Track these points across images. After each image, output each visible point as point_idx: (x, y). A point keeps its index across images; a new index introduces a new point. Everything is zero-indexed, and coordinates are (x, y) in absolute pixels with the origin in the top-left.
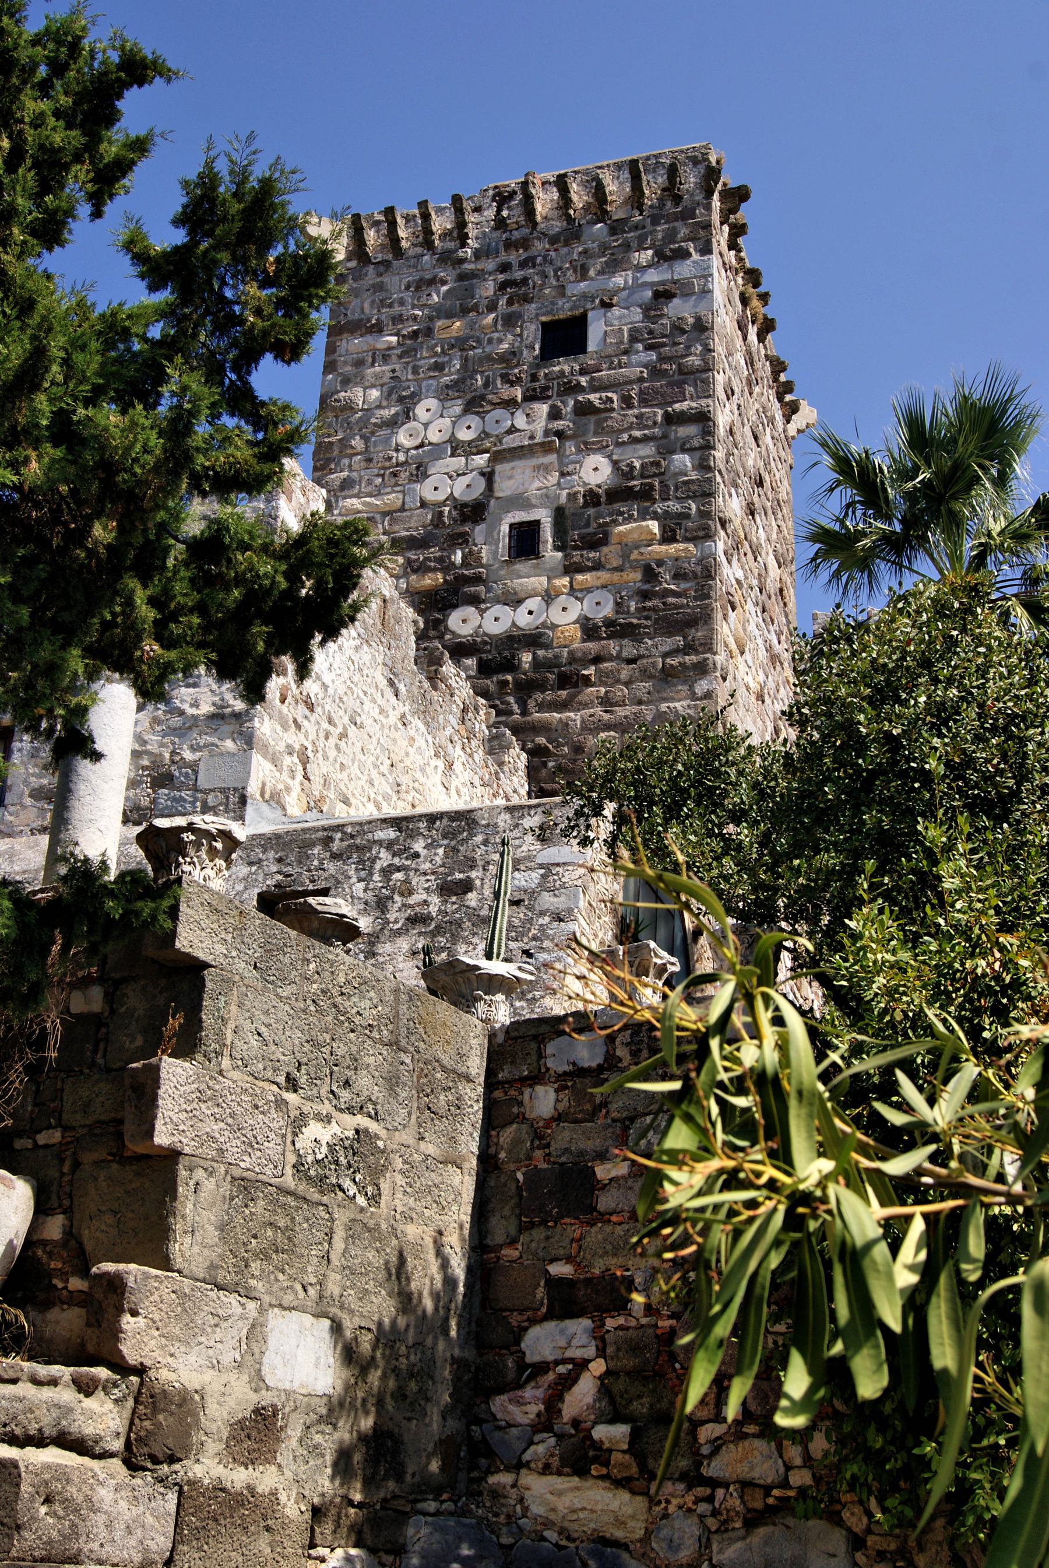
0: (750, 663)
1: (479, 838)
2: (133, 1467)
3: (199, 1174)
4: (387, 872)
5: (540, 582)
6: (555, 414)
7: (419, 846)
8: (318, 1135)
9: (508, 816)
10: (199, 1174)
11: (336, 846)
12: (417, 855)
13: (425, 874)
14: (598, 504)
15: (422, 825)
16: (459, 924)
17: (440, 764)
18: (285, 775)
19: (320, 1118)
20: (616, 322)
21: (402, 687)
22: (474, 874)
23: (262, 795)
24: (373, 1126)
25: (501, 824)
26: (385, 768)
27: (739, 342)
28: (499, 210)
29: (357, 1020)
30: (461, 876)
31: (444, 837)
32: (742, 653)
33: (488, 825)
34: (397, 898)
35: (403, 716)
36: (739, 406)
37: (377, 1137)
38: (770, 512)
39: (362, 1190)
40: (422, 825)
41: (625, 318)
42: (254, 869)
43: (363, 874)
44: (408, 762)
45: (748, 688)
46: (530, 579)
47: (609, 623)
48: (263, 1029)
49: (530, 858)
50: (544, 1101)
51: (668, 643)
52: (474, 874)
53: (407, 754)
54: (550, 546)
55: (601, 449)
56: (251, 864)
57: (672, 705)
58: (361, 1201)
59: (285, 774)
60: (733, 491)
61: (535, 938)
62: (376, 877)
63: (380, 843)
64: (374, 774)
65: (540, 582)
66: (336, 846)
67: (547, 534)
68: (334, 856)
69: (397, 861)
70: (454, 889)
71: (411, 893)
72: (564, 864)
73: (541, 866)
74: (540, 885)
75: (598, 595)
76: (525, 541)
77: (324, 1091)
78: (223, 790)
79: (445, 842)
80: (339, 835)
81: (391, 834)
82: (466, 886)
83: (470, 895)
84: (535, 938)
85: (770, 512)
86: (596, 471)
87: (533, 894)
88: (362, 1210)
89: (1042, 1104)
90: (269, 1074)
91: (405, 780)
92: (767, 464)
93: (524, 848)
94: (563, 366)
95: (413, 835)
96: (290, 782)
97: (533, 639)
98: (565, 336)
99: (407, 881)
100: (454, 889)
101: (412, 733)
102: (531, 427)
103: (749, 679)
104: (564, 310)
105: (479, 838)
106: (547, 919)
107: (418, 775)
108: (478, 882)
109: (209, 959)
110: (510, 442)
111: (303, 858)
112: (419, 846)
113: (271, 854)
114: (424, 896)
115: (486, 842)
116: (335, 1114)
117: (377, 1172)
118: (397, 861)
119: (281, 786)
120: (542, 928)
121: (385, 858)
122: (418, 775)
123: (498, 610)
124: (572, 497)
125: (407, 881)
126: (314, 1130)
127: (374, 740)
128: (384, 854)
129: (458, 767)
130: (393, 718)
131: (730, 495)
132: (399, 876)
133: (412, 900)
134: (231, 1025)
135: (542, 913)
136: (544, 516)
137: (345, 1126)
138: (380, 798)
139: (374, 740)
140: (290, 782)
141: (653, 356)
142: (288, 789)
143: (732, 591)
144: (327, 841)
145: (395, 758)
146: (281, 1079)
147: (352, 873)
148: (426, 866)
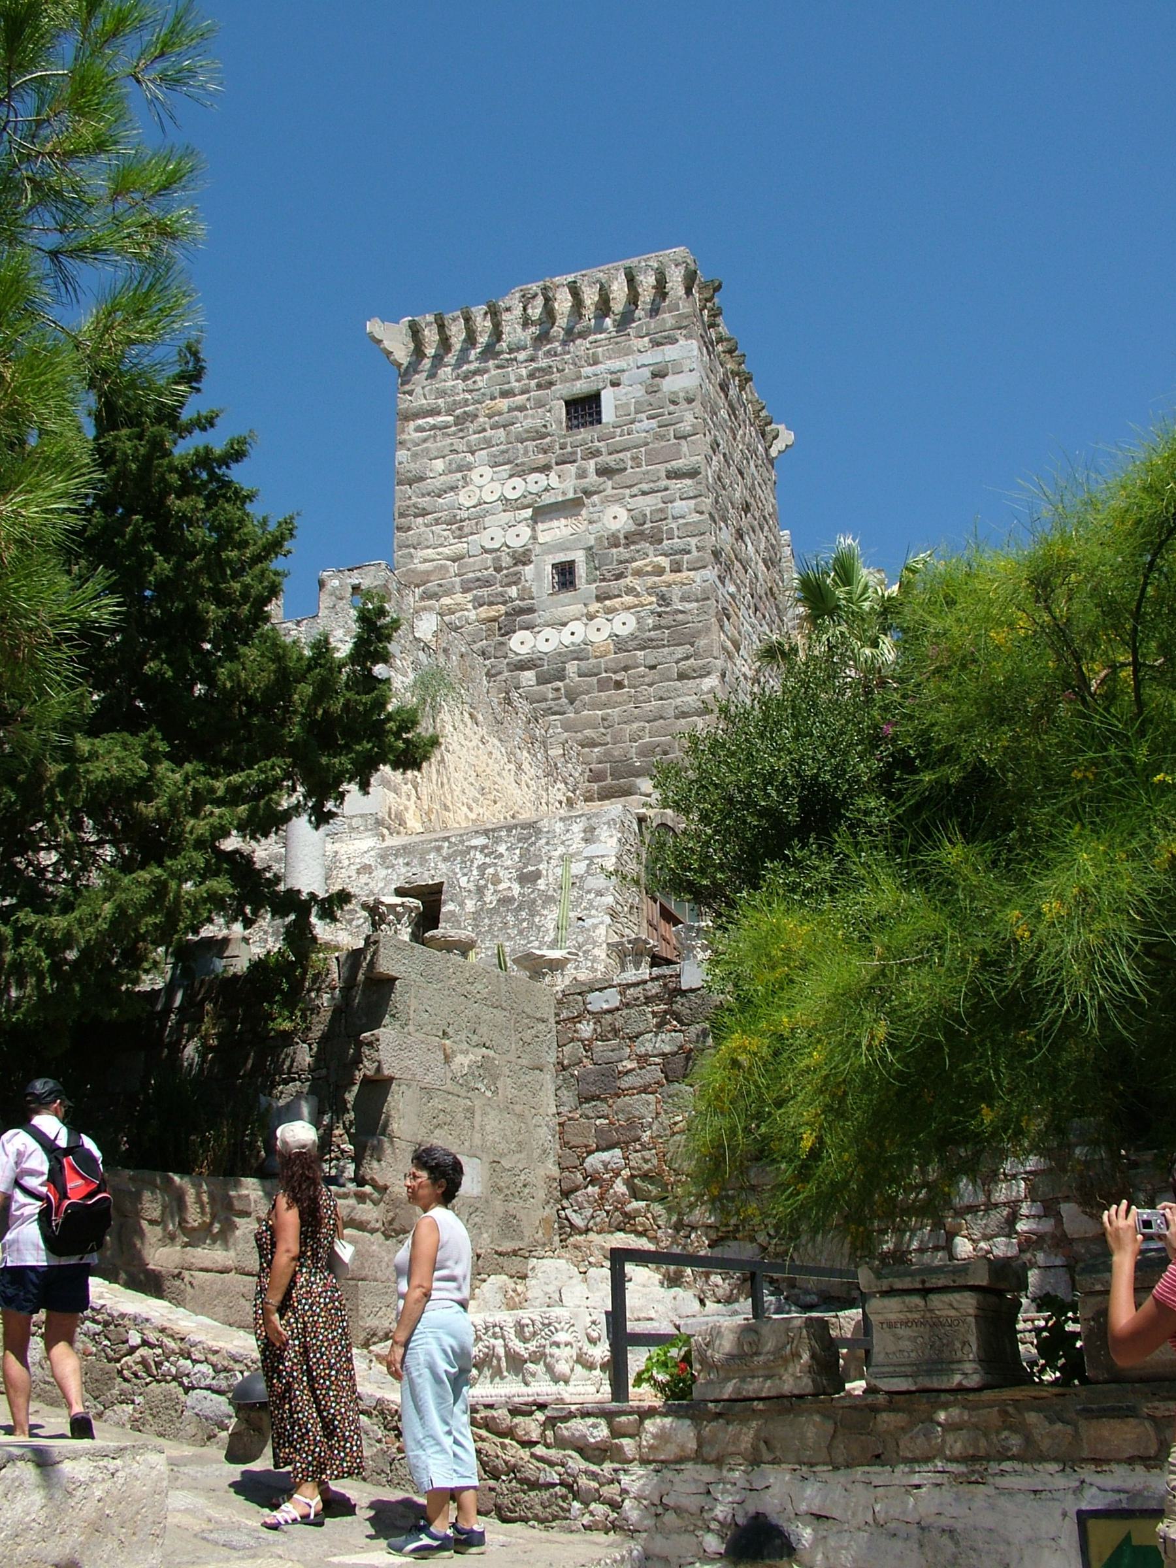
0: (746, 657)
1: (543, 841)
2: (387, 1237)
3: (404, 1087)
4: (482, 868)
5: (578, 608)
6: (582, 474)
7: (502, 849)
8: (463, 1061)
9: (562, 824)
10: (404, 1087)
11: (445, 852)
12: (501, 855)
13: (507, 869)
14: (617, 546)
15: (503, 833)
16: (534, 901)
17: (512, 766)
18: (404, 800)
19: (462, 1052)
20: (623, 398)
21: (480, 717)
22: (541, 867)
23: (390, 817)
24: (491, 1053)
25: (558, 830)
26: (472, 780)
27: (722, 402)
28: (525, 309)
29: (478, 996)
30: (533, 868)
31: (519, 840)
32: (738, 650)
33: (548, 832)
34: (489, 885)
35: (483, 737)
36: (724, 455)
37: (494, 1059)
38: (757, 528)
39: (488, 1088)
40: (503, 833)
41: (630, 392)
42: (390, 871)
43: (465, 870)
44: (488, 771)
45: (746, 678)
46: (568, 605)
47: (633, 637)
48: (428, 1008)
49: (579, 853)
50: (586, 1029)
51: (680, 652)
52: (541, 867)
53: (487, 765)
54: (583, 580)
55: (619, 500)
56: (387, 868)
57: (684, 699)
58: (489, 1094)
59: (404, 797)
60: (722, 524)
61: (586, 909)
62: (475, 872)
63: (475, 847)
64: (466, 785)
65: (578, 608)
66: (445, 852)
67: (581, 570)
68: (445, 860)
69: (488, 860)
70: (528, 879)
71: (499, 882)
72: (603, 856)
73: (587, 858)
74: (587, 872)
75: (625, 616)
76: (565, 575)
77: (464, 1038)
78: (362, 816)
79: (520, 845)
80: (446, 844)
81: (481, 841)
82: (537, 875)
83: (539, 882)
84: (586, 909)
85: (757, 528)
86: (617, 519)
87: (581, 878)
88: (489, 1099)
89: (1175, 936)
90: (434, 1032)
91: (487, 784)
92: (751, 489)
93: (574, 846)
94: (584, 434)
95: (497, 841)
96: (407, 803)
97: (578, 654)
98: (584, 409)
99: (496, 875)
100: (528, 879)
101: (490, 749)
102: (562, 486)
103: (745, 669)
104: (580, 388)
105: (543, 841)
106: (593, 895)
107: (497, 779)
108: (544, 872)
109: (397, 975)
110: (548, 499)
111: (423, 861)
112: (502, 849)
113: (401, 861)
114: (509, 884)
115: (547, 844)
116: (471, 1049)
117: (495, 1078)
118: (488, 860)
119: (401, 808)
120: (590, 902)
121: (480, 858)
122: (497, 779)
123: (548, 632)
124: (599, 539)
125: (496, 875)
126: (459, 1059)
127: (463, 760)
128: (478, 855)
129: (526, 766)
130: (476, 741)
131: (720, 529)
132: (491, 870)
133: (501, 887)
134: (412, 1008)
135: (589, 892)
136: (579, 557)
137: (476, 1055)
138: (471, 802)
139: (463, 760)
140: (407, 803)
141: (654, 423)
142: (406, 809)
143: (726, 605)
144: (438, 849)
145: (479, 770)
146: (440, 1034)
147: (457, 870)
148: (509, 862)
